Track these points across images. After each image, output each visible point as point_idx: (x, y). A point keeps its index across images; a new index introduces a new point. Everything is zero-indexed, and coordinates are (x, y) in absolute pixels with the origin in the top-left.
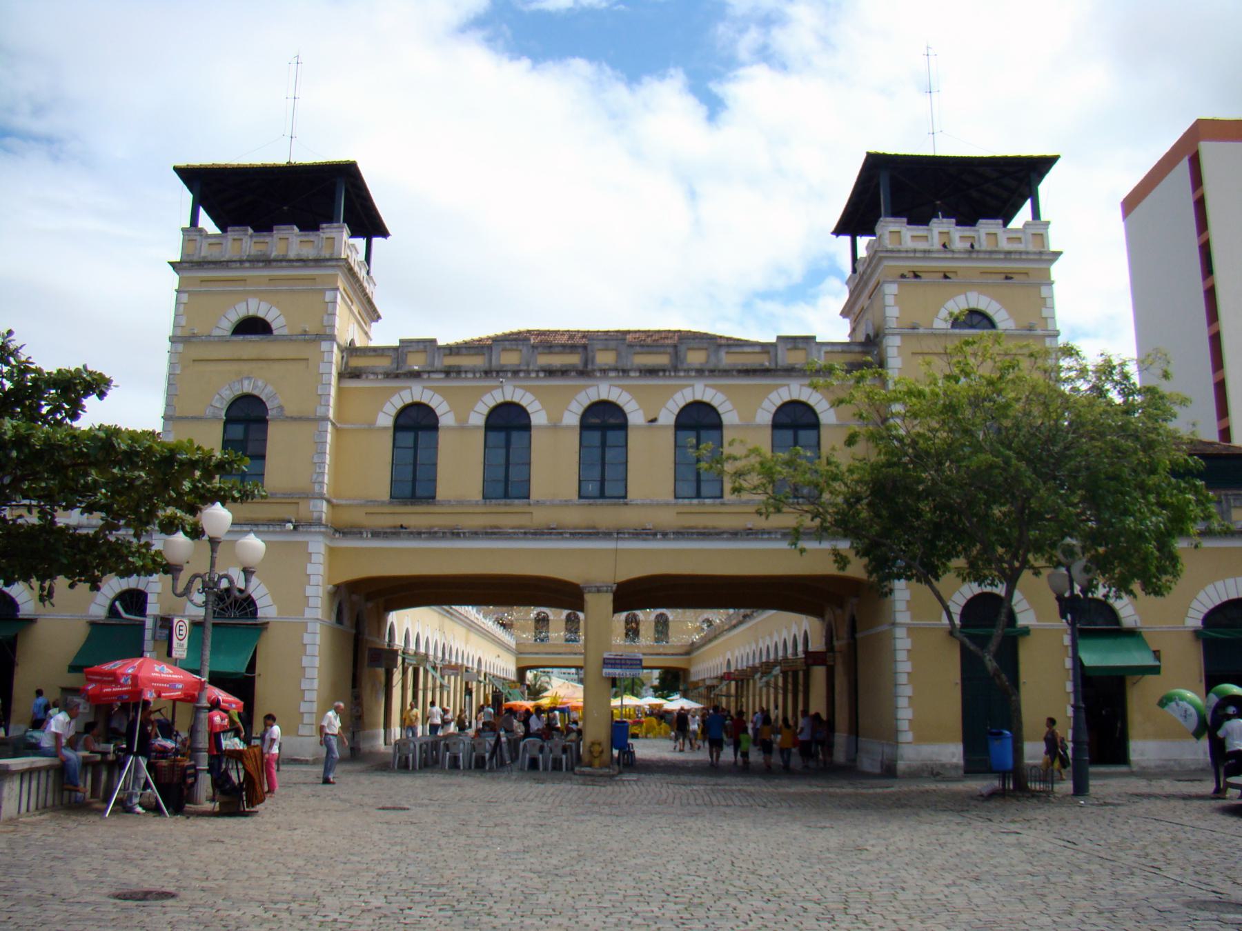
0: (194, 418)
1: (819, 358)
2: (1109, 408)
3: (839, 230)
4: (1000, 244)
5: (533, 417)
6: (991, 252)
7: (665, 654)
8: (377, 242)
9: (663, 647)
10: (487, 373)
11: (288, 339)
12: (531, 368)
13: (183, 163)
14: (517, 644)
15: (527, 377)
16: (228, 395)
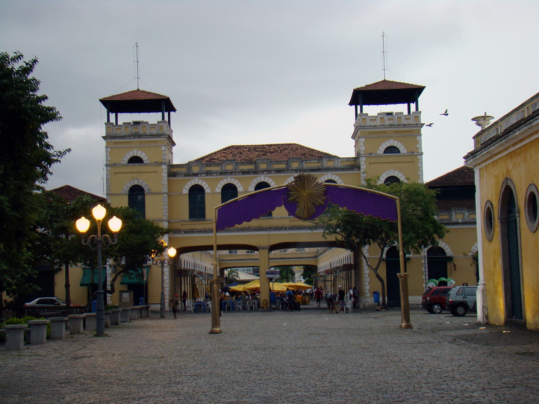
0: (118, 194)
1: (338, 164)
3: (351, 104)
4: (402, 121)
5: (238, 189)
6: (398, 125)
8: (172, 113)
10: (221, 174)
11: (150, 164)
12: (237, 171)
13: (102, 98)
15: (236, 174)
16: (129, 185)
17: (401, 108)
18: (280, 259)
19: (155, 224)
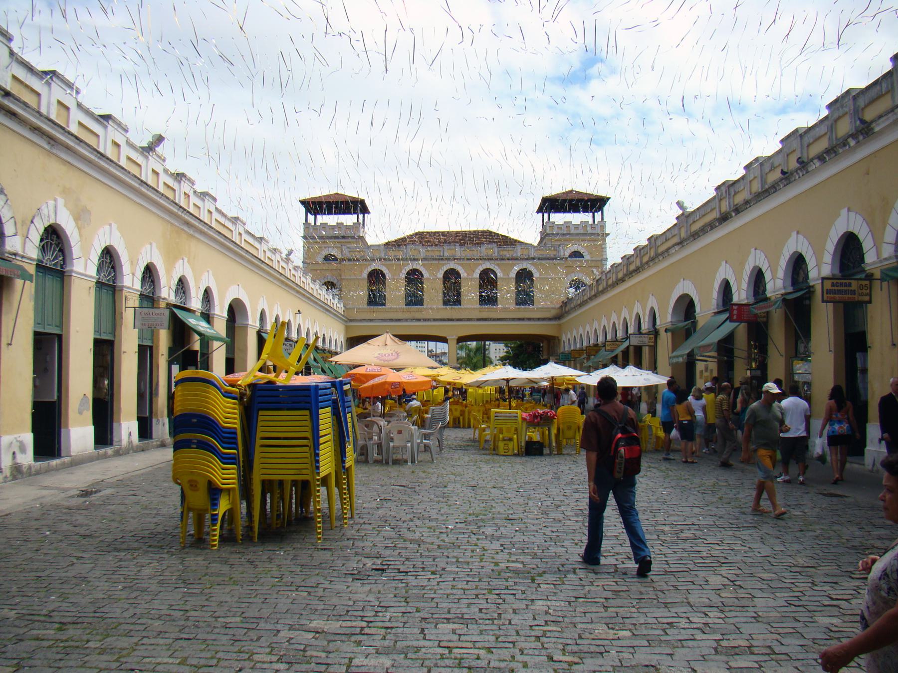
2: (292, 494)
3: (538, 212)
7: (529, 319)
8: (366, 215)
9: (526, 311)
13: (302, 199)
17: (586, 217)
18: (478, 320)
19: (769, 339)
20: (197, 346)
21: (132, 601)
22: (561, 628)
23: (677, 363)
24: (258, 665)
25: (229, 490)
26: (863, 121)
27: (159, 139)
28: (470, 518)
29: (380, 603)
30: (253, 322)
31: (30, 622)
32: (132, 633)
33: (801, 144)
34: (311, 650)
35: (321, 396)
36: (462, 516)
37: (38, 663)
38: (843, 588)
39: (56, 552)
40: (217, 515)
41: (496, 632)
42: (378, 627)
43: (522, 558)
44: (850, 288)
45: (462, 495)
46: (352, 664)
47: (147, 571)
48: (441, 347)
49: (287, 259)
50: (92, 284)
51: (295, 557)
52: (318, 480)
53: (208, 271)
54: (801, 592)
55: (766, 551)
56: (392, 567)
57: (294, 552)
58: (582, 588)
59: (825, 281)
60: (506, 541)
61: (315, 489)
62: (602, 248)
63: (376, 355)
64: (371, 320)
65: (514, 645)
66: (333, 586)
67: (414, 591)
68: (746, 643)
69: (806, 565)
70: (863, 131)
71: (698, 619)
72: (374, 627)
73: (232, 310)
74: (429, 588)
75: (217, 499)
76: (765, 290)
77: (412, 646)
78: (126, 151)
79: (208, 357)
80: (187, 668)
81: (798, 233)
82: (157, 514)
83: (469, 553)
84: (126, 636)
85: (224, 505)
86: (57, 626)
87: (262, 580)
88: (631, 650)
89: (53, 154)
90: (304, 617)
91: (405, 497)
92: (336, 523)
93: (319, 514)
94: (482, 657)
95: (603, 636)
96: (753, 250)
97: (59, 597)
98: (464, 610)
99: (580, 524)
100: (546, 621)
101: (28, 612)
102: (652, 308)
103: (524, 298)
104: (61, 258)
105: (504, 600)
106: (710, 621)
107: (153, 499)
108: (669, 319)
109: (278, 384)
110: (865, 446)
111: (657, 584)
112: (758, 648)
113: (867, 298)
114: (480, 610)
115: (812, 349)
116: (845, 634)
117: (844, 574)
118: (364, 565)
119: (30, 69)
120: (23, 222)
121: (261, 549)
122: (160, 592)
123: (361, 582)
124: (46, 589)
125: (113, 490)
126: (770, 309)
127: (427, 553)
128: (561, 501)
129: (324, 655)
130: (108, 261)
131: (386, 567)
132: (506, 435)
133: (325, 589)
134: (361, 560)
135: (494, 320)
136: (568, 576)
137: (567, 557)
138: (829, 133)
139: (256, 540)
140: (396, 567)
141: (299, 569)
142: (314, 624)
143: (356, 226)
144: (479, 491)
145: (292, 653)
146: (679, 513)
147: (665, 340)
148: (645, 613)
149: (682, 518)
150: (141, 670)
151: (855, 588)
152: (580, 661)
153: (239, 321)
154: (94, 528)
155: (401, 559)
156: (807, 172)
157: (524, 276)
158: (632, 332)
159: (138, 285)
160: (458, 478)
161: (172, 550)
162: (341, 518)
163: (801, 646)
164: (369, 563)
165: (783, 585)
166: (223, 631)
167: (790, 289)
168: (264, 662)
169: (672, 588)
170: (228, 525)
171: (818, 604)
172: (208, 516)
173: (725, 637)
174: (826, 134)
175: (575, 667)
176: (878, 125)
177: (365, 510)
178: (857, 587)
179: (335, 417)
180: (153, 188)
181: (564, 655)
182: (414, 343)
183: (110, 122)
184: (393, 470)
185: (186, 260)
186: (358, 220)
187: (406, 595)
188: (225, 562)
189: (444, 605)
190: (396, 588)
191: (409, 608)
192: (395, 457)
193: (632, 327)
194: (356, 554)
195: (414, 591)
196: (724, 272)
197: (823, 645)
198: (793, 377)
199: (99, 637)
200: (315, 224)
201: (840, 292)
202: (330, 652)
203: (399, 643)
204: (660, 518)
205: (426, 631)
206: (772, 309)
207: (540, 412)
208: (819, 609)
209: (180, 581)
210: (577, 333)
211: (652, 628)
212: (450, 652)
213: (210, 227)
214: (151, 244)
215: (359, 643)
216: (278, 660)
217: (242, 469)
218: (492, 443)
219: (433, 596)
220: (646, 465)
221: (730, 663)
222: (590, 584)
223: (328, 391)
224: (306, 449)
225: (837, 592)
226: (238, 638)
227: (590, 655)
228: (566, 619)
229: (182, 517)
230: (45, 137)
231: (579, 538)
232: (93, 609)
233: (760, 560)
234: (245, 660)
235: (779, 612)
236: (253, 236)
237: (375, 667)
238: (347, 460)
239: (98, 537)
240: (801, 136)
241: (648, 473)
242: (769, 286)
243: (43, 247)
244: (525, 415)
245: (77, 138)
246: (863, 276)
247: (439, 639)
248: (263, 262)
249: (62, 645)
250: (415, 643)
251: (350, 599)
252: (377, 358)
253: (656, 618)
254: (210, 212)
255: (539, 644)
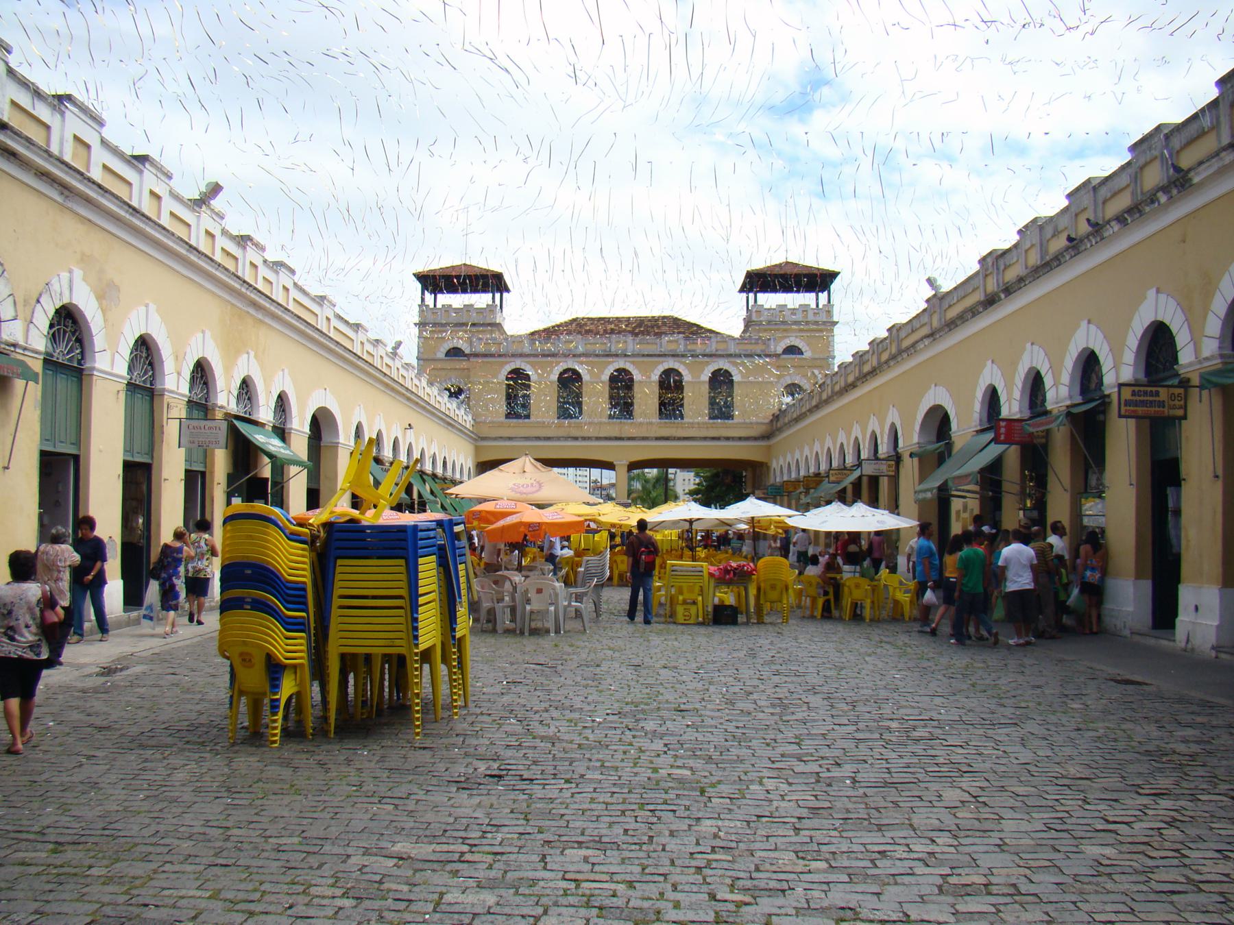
3: (742, 290)
7: (728, 439)
8: (505, 295)
14: (476, 422)
17: (807, 298)
18: (657, 439)
19: (1049, 467)
20: (266, 472)
21: (156, 815)
22: (733, 856)
23: (924, 500)
24: (316, 901)
25: (295, 667)
26: (1177, 169)
27: (216, 189)
28: (627, 709)
29: (491, 819)
30: (345, 438)
31: (15, 841)
32: (150, 858)
33: (1095, 201)
34: (390, 882)
35: (421, 539)
36: (616, 705)
37: (21, 895)
38: (1124, 807)
39: (59, 749)
40: (278, 700)
41: (643, 861)
42: (483, 853)
43: (691, 763)
44: (1157, 399)
45: (620, 677)
46: (443, 901)
47: (180, 776)
48: (608, 477)
49: (394, 354)
50: (123, 387)
51: (383, 759)
52: (416, 654)
53: (283, 370)
54: (1067, 812)
55: (1026, 756)
56: (513, 772)
57: (381, 752)
58: (767, 803)
59: (1123, 389)
60: (673, 740)
61: (412, 666)
62: (828, 345)
63: (511, 485)
64: (510, 439)
65: (666, 878)
66: (428, 798)
67: (538, 806)
68: (983, 880)
69: (1078, 775)
70: (1178, 183)
71: (920, 847)
72: (479, 852)
73: (316, 423)
74: (559, 800)
75: (278, 679)
76: (1044, 400)
77: (528, 879)
78: (169, 205)
79: (283, 487)
80: (220, 903)
81: (1089, 322)
82: (201, 700)
83: (619, 756)
84: (142, 860)
85: (288, 687)
86: (51, 846)
87: (332, 790)
88: (825, 887)
89: (68, 208)
90: (385, 837)
91: (542, 680)
92: (441, 713)
93: (417, 701)
94: (619, 894)
95: (788, 868)
96: (1028, 345)
97: (58, 808)
98: (604, 832)
99: (777, 718)
100: (713, 847)
101: (15, 828)
102: (893, 425)
103: (721, 411)
104: (78, 351)
105: (659, 818)
106: (937, 849)
107: (198, 679)
108: (915, 439)
109: (364, 523)
110: (1175, 615)
111: (871, 799)
112: (997, 887)
113: (1180, 413)
114: (626, 831)
115: (1106, 482)
116: (1119, 869)
117: (1129, 788)
118: (476, 769)
119: (37, 93)
120: (26, 302)
121: (338, 747)
122: (195, 803)
123: (468, 792)
124: (41, 799)
125: (146, 667)
126: (1051, 426)
127: (562, 755)
128: (754, 687)
129: (405, 888)
130: (144, 355)
131: (505, 772)
132: (688, 596)
133: (418, 801)
134: (471, 763)
135: (679, 439)
136: (751, 787)
137: (753, 762)
138: (1132, 185)
139: (332, 735)
140: (518, 773)
141: (386, 774)
142: (398, 848)
143: (491, 309)
144: (643, 672)
145: (363, 885)
146: (913, 704)
147: (910, 468)
148: (850, 838)
149: (916, 711)
150: (156, 906)
151: (1142, 807)
152: (753, 901)
153: (326, 439)
154: (113, 717)
155: (525, 762)
156: (1102, 239)
157: (720, 380)
158: (866, 457)
159: (185, 388)
160: (617, 654)
161: (218, 748)
162: (450, 707)
163: (1057, 884)
164: (482, 767)
165: (1044, 803)
166: (274, 855)
167: (1078, 399)
168: (324, 897)
169: (891, 805)
170: (296, 714)
171: (1088, 828)
172: (266, 701)
173: (955, 871)
174: (1128, 186)
175: (745, 909)
176: (1197, 174)
177: (484, 696)
178: (1145, 806)
179: (441, 569)
180: (206, 256)
181: (732, 892)
182: (571, 470)
183: (147, 165)
184: (529, 643)
185: (252, 354)
186: (494, 301)
187: (527, 810)
188: (287, 764)
189: (578, 824)
190: (515, 801)
191: (528, 828)
192: (533, 625)
193: (866, 451)
194: (466, 754)
195: (538, 806)
196: (990, 375)
197: (1087, 884)
198: (1082, 520)
199: (105, 862)
200: (435, 305)
201: (1143, 403)
202: (415, 885)
203: (509, 874)
204: (887, 710)
205: (548, 859)
206: (1053, 426)
207: (734, 564)
208: (1089, 835)
209: (224, 789)
210: (793, 458)
211: (857, 858)
212: (577, 887)
213: (286, 309)
214: (203, 332)
215: (455, 873)
216: (344, 894)
217: (313, 638)
218: (668, 607)
219: (562, 811)
220: (878, 639)
221: (957, 907)
222: (780, 798)
223: (432, 534)
224: (401, 612)
225: (1116, 812)
226: (293, 864)
227: (767, 893)
228: (740, 844)
229: (231, 704)
230: (56, 185)
231: (773, 737)
232: (101, 825)
233: (1017, 768)
234: (298, 894)
235: (1032, 839)
236: (346, 322)
237: (473, 905)
238: (458, 627)
239: (120, 730)
240: (1094, 188)
241: (879, 650)
242: (1050, 395)
243: (54, 335)
244: (712, 569)
245: (100, 186)
246: (1175, 381)
247: (564, 869)
248: (359, 357)
249: (55, 871)
250: (531, 874)
251: (450, 815)
252: (512, 489)
253: (864, 845)
254: (286, 289)
255: (699, 877)
